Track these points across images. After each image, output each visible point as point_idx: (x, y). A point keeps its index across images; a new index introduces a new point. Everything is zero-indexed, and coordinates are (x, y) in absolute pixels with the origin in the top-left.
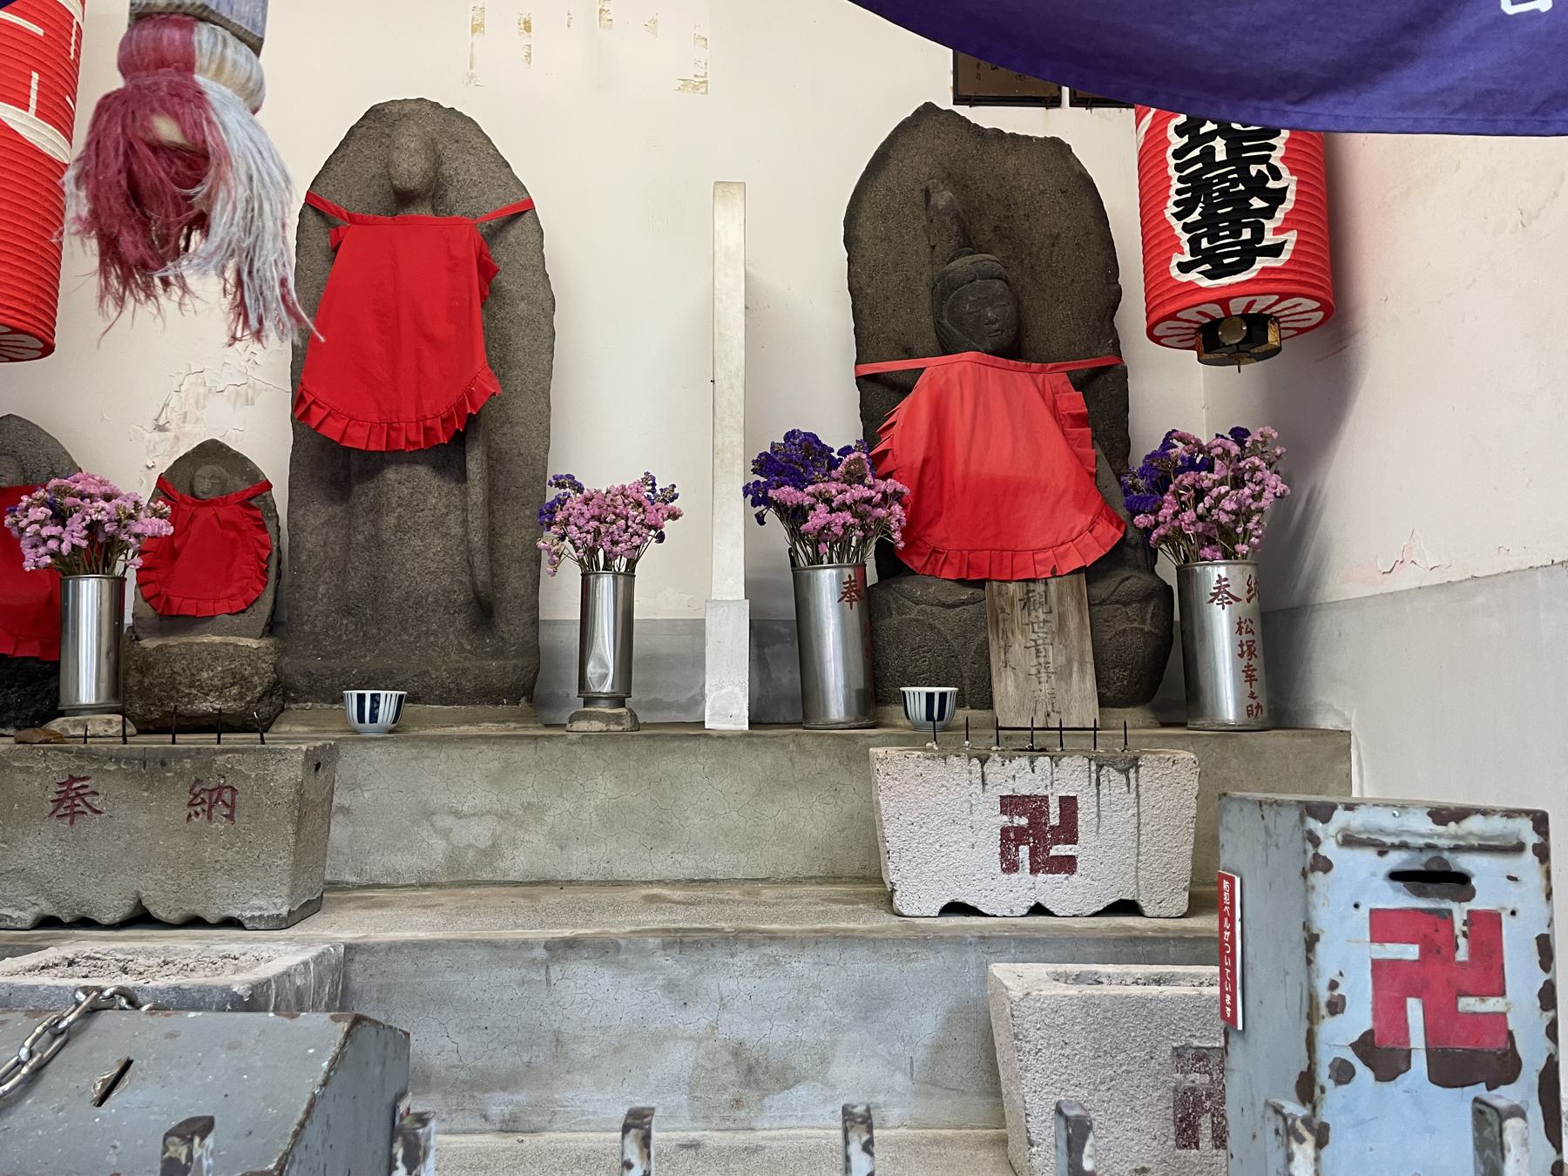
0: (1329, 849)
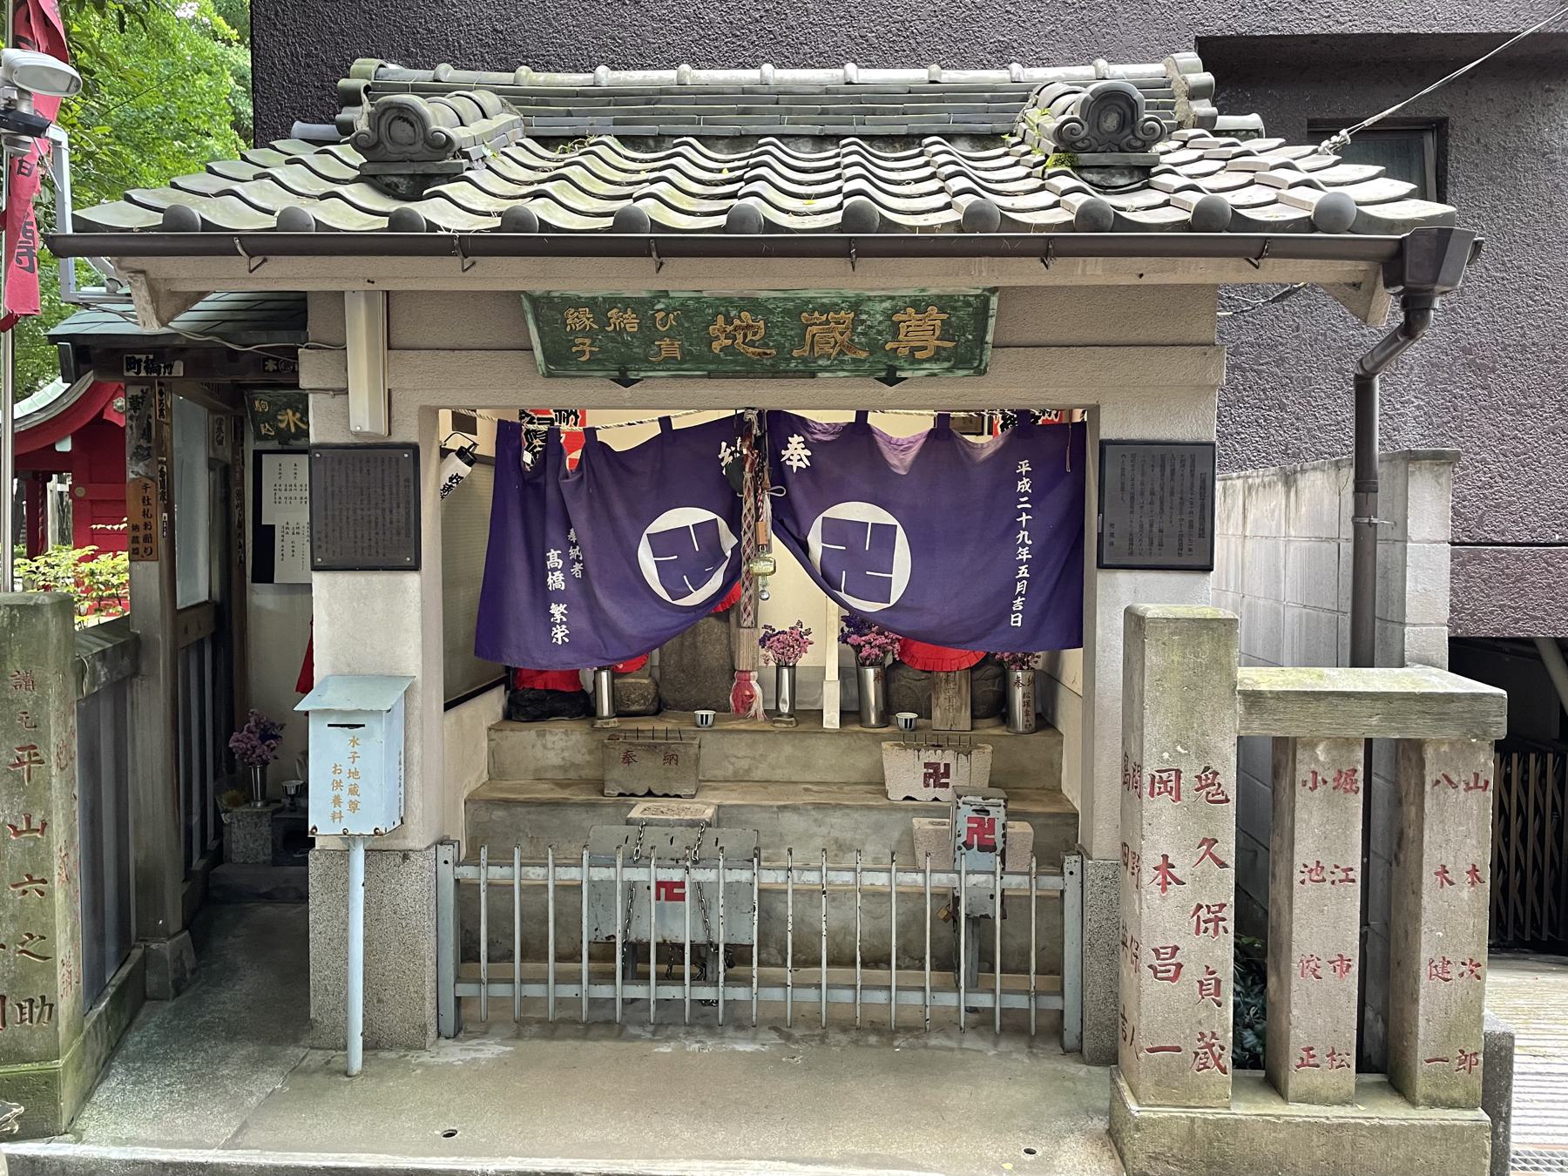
0: (960, 805)
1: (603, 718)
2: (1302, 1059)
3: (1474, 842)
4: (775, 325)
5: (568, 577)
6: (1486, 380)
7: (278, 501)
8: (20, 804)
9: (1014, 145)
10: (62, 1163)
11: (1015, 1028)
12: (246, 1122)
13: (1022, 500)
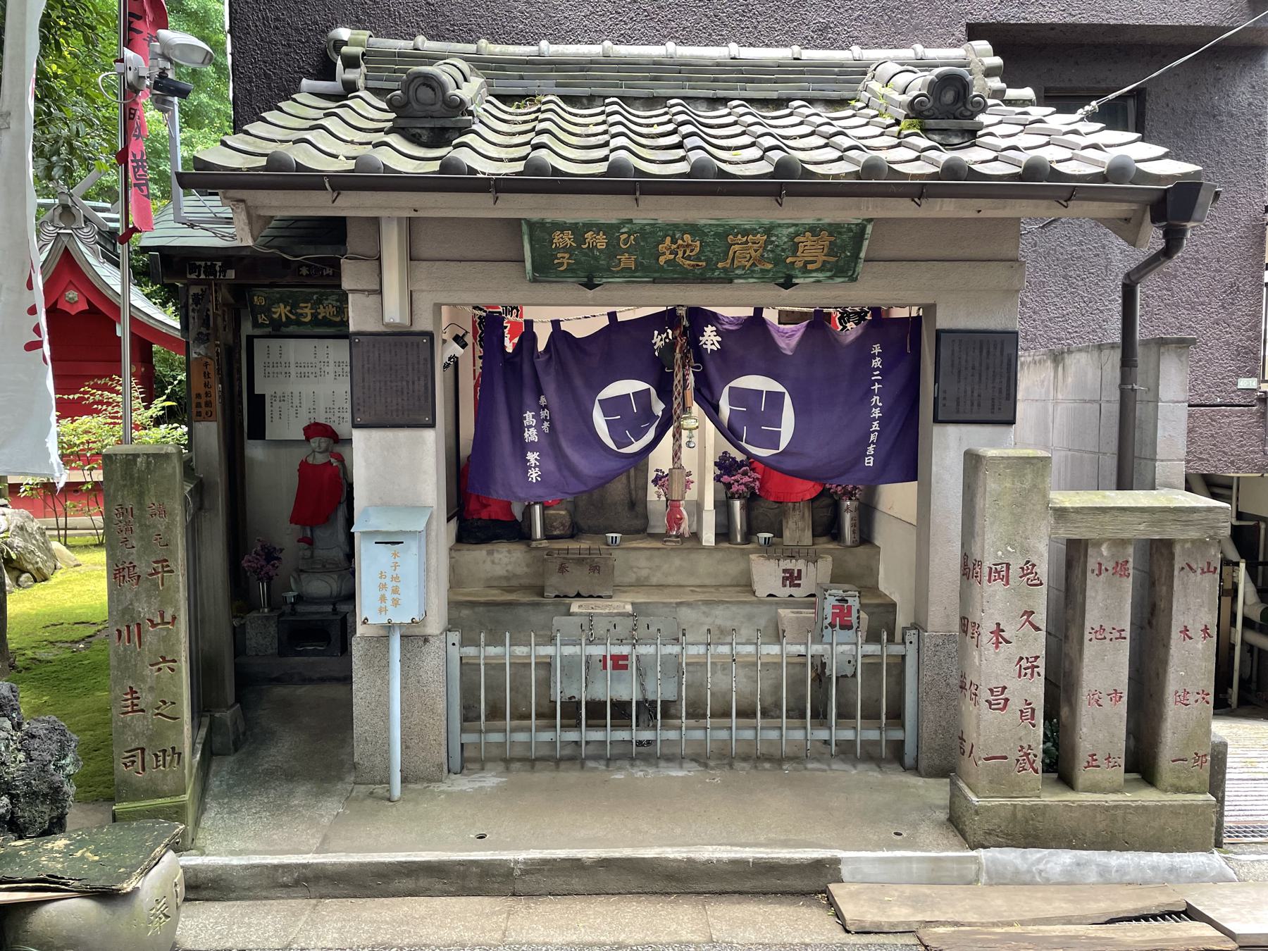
0: (827, 596)
1: (536, 540)
2: (1088, 762)
3: (1206, 609)
4: (708, 244)
5: (540, 432)
6: (1170, 284)
7: (267, 375)
8: (155, 603)
9: (860, 109)
10: (195, 870)
11: (869, 756)
12: (326, 835)
13: (875, 373)
